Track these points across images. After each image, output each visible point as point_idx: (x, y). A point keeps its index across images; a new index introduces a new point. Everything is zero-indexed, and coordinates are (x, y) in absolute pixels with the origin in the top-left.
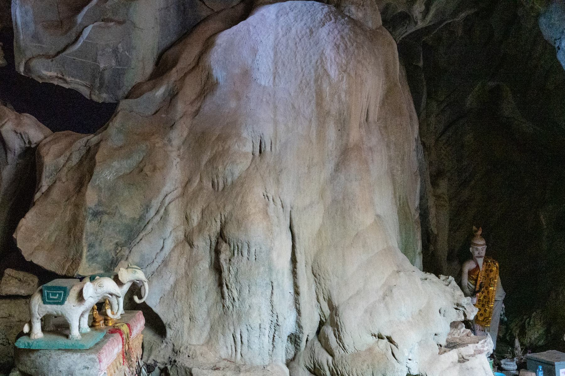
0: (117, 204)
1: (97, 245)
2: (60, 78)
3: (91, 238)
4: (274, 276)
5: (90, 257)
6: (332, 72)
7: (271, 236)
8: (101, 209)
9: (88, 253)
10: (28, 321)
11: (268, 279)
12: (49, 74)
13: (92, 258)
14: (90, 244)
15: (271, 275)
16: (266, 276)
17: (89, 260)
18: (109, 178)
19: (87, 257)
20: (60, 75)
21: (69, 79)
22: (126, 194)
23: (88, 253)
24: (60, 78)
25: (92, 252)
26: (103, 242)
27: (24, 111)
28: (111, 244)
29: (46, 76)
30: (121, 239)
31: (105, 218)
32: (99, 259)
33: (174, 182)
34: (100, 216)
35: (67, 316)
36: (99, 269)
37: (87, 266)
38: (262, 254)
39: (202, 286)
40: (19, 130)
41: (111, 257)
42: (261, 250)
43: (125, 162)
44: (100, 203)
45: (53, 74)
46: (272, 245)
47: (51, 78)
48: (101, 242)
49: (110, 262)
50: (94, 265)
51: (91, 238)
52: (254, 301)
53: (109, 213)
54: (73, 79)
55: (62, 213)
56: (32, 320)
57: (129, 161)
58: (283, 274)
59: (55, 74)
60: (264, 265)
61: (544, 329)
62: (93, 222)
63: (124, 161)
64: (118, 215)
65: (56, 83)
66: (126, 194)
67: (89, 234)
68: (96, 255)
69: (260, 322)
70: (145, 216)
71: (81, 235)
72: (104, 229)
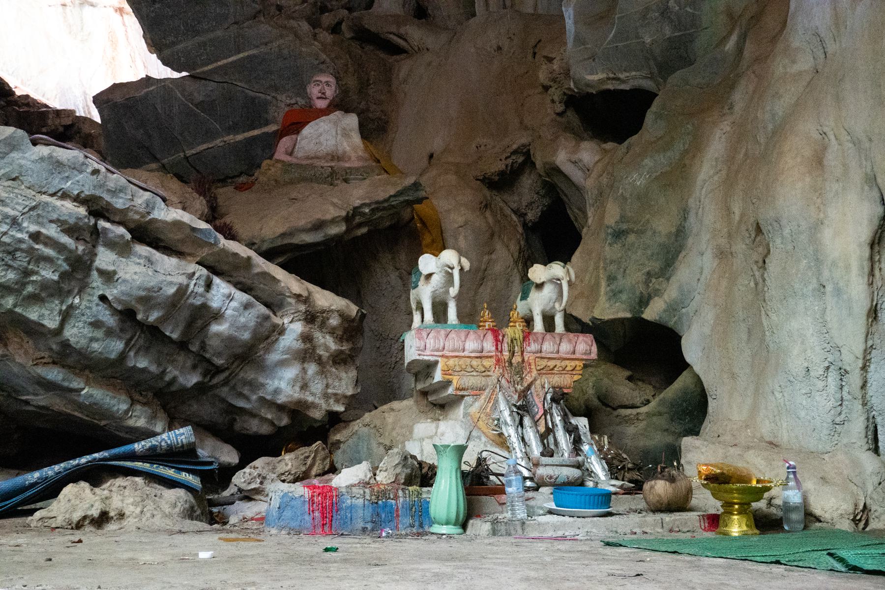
0: (648, 216)
1: (619, 277)
2: (614, 79)
3: (613, 268)
4: (826, 273)
7: (819, 201)
8: (624, 227)
9: (608, 289)
11: (815, 281)
12: (595, 77)
13: (614, 295)
14: (610, 276)
15: (819, 273)
16: (810, 274)
17: (609, 299)
18: (638, 183)
19: (606, 293)
20: (611, 76)
21: (622, 76)
22: (662, 200)
23: (608, 289)
24: (614, 79)
25: (613, 287)
26: (627, 272)
28: (639, 274)
29: (593, 81)
30: (655, 265)
31: (632, 238)
32: (624, 297)
33: (714, 163)
34: (624, 237)
36: (624, 310)
37: (607, 305)
38: (437, 144)
39: (741, 319)
40: (575, 157)
41: (638, 293)
42: (800, 229)
43: (662, 156)
44: (623, 218)
45: (601, 76)
46: (822, 215)
47: (601, 81)
50: (617, 304)
51: (613, 268)
52: (794, 325)
53: (638, 230)
54: (628, 74)
57: (669, 154)
58: (848, 268)
59: (605, 75)
60: (806, 257)
62: (615, 245)
63: (659, 155)
64: (649, 233)
65: (610, 87)
66: (662, 200)
67: (608, 261)
68: (620, 292)
69: (806, 365)
70: (684, 227)
72: (630, 253)
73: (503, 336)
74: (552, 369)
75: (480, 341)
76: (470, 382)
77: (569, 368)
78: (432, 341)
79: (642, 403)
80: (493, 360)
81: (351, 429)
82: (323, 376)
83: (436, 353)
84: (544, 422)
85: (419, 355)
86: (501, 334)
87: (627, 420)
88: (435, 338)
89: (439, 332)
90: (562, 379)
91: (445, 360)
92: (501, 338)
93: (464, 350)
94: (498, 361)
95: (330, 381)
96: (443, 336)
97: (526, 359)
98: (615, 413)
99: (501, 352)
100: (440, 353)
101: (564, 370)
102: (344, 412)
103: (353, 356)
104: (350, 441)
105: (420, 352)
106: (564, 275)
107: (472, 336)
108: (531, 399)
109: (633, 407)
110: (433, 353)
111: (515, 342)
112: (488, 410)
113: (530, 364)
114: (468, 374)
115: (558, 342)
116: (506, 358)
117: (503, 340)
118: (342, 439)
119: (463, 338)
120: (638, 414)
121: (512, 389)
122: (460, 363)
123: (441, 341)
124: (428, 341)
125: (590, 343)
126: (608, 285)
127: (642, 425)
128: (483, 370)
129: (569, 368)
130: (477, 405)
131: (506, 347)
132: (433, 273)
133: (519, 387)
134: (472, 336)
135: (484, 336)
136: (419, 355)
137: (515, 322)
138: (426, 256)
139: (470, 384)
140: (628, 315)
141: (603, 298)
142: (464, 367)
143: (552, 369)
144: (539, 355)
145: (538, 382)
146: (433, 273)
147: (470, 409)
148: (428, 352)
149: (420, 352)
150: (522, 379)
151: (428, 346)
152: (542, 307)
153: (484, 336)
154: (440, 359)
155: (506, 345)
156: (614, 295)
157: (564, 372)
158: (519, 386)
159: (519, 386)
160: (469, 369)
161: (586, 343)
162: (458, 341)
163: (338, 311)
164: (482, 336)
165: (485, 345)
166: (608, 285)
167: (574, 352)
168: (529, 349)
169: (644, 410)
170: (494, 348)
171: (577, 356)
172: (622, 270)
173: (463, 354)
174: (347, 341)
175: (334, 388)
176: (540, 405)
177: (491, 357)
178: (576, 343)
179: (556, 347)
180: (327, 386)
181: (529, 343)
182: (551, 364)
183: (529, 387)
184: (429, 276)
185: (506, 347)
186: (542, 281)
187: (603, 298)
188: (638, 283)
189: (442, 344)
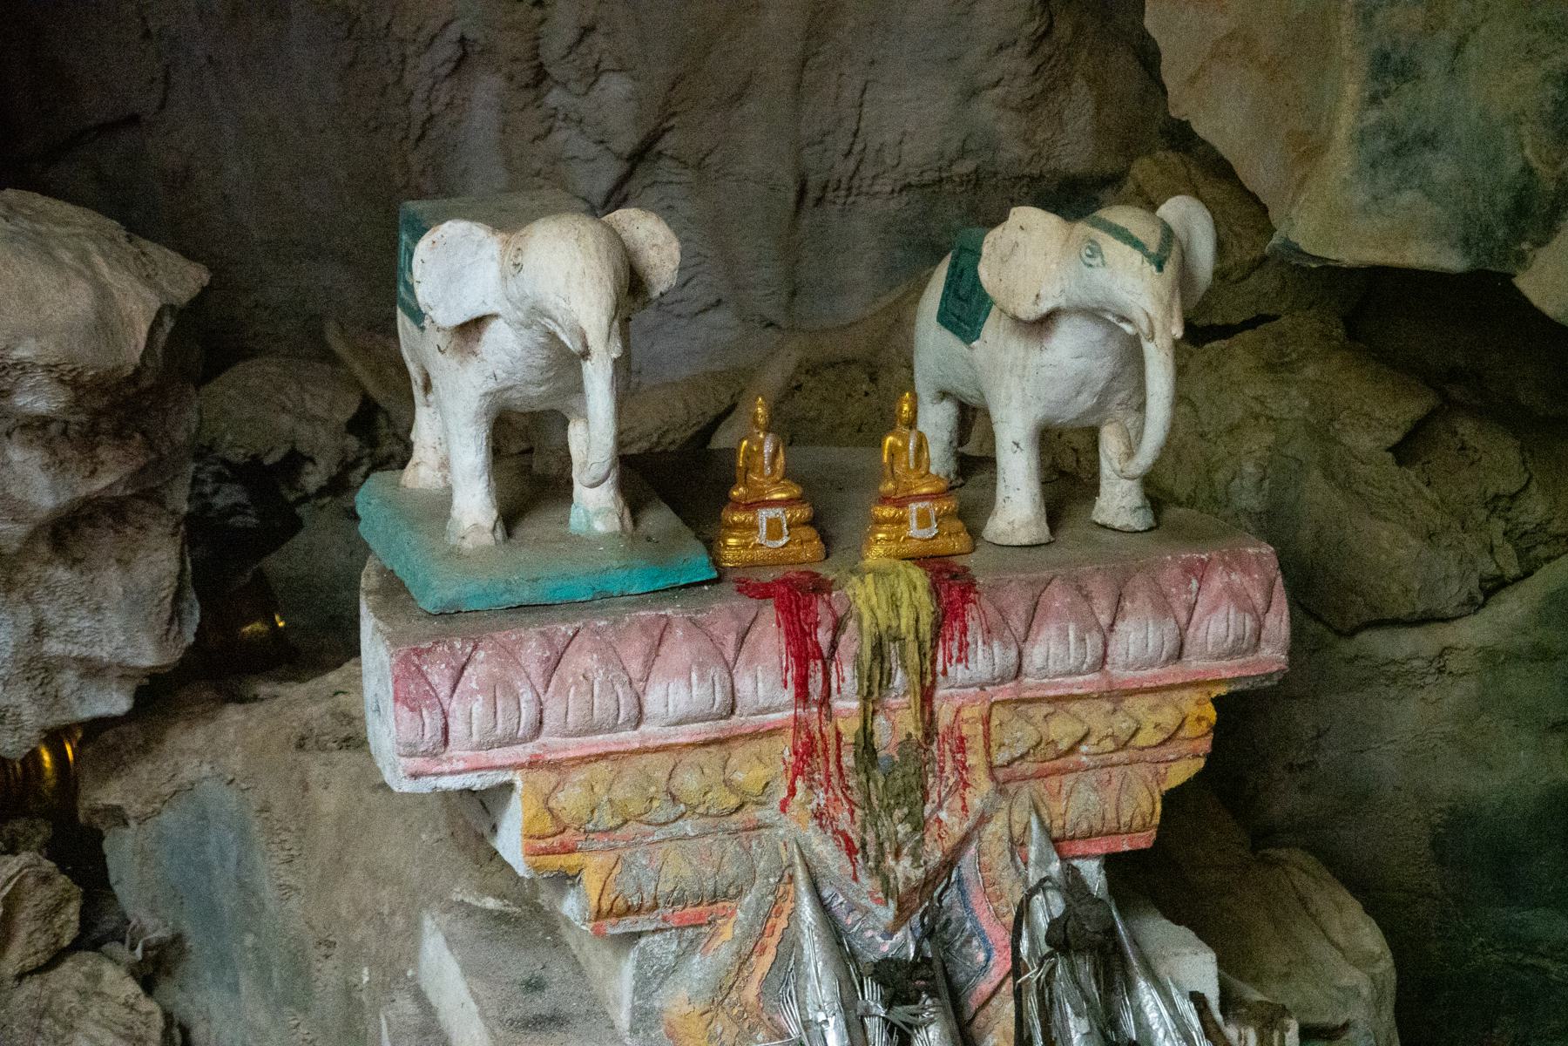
1: (1433, 68)
5: (1382, 143)
6: (192, 614)
9: (1373, 116)
10: (648, 317)
19: (1361, 138)
23: (1373, 116)
25: (1393, 110)
26: (1471, 52)
27: (531, 217)
32: (1443, 169)
35: (1386, 632)
37: (1361, 197)
41: (1512, 166)
48: (1458, 50)
49: (1504, 200)
50: (1407, 197)
55: (817, 54)
56: (630, 244)
61: (128, 468)
62: (21, 577)
68: (1428, 141)
69: (910, 128)
71: (138, 748)
73: (838, 627)
74: (1072, 750)
75: (717, 672)
76: (669, 872)
77: (1147, 737)
78: (478, 707)
79: (1471, 600)
80: (784, 747)
81: (167, 767)
82: (15, 596)
83: (500, 756)
84: (1010, 1007)
85: (415, 776)
86: (826, 620)
87: (1396, 675)
88: (499, 688)
89: (509, 654)
90: (1111, 793)
91: (545, 779)
92: (823, 637)
93: (639, 719)
94: (808, 752)
95: (52, 615)
96: (535, 669)
97: (944, 717)
98: (1347, 648)
99: (825, 702)
100: (522, 752)
101: (1124, 746)
102: (127, 718)
103: (154, 490)
104: (168, 817)
105: (417, 763)
106: (1156, 312)
107: (679, 649)
108: (958, 911)
109: (1427, 619)
110: (485, 757)
111: (893, 649)
112: (752, 991)
113: (961, 745)
114: (659, 834)
115: (1104, 619)
116: (850, 727)
117: (834, 645)
118: (134, 808)
119: (635, 668)
120: (1445, 651)
121: (868, 883)
122: (619, 793)
123: (526, 696)
124: (455, 707)
125: (1258, 598)
126: (1374, 100)
127: (1457, 693)
128: (734, 801)
129: (1147, 737)
130: (699, 968)
131: (847, 677)
132: (495, 316)
133: (904, 870)
134: (679, 649)
135: (741, 640)
136: (415, 776)
137: (901, 503)
138: (452, 230)
139: (665, 888)
140: (1453, 261)
141: (1341, 160)
142: (635, 807)
143: (1072, 750)
144: (1007, 691)
145: (996, 827)
146: (495, 316)
147: (668, 989)
148: (459, 753)
149: (417, 763)
150: (919, 825)
151: (457, 728)
152: (1037, 412)
153: (741, 640)
154: (518, 778)
155: (848, 671)
156: (1397, 152)
157: (1122, 756)
158: (906, 862)
159: (906, 862)
160: (662, 810)
161: (1239, 599)
162: (609, 686)
163: (49, 368)
164: (731, 639)
165: (744, 685)
166: (1374, 100)
167: (1179, 654)
168: (958, 672)
169: (1472, 632)
170: (789, 694)
171: (1195, 665)
172: (1446, 38)
173: (629, 738)
174: (120, 435)
175: (70, 637)
176: (1000, 937)
177: (772, 732)
178: (1191, 610)
179: (1093, 641)
180: (39, 631)
181: (963, 647)
182: (1062, 730)
183: (950, 863)
184: (472, 329)
185: (847, 677)
186: (1045, 306)
187: (1341, 160)
188: (1516, 120)
189: (528, 713)
